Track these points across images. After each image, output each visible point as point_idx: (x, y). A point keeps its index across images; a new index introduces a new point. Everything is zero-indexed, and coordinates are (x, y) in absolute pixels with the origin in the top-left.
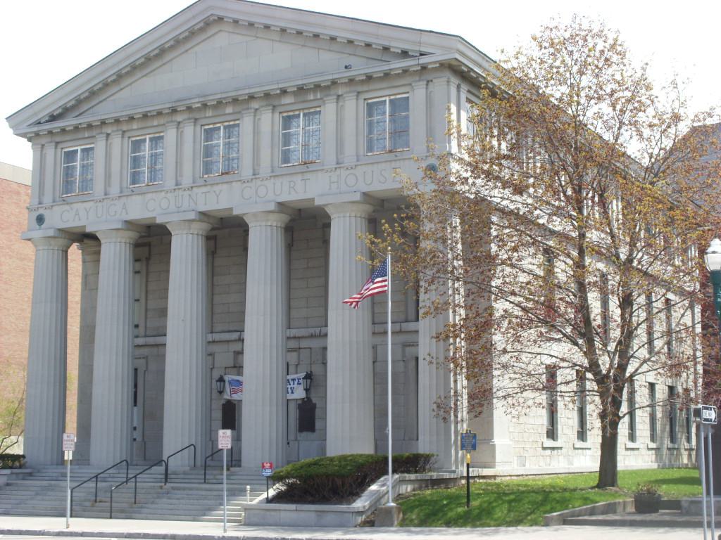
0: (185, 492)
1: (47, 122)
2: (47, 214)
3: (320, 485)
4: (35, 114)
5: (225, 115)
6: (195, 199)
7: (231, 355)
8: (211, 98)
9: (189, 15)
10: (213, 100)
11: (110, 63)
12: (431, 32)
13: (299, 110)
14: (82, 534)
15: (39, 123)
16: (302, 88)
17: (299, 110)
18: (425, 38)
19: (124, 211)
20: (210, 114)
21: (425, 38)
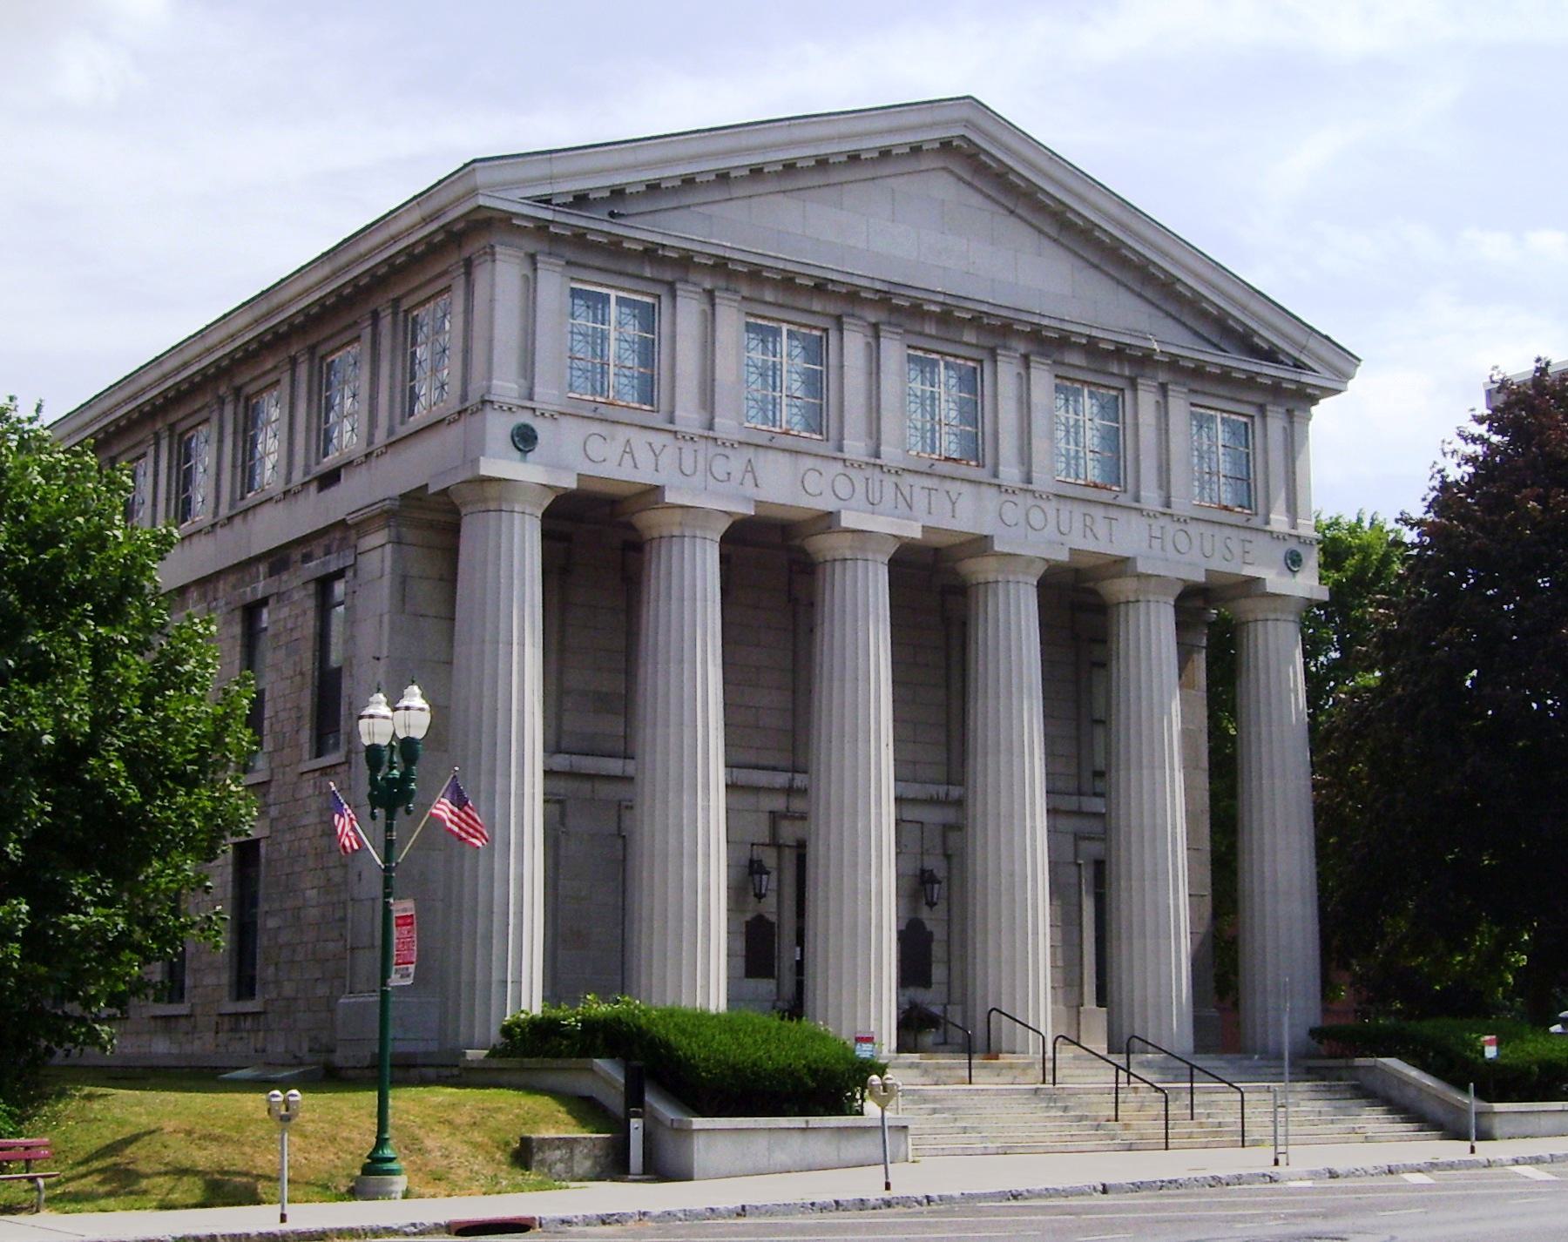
0: (1472, 1172)
1: (565, 205)
2: (542, 428)
3: (641, 1083)
4: (551, 179)
5: (1063, 364)
6: (900, 498)
7: (764, 821)
8: (1025, 317)
9: (927, 117)
10: (969, 310)
11: (746, 140)
12: (1327, 338)
13: (1085, 382)
14: (376, 1233)
15: (548, 202)
16: (792, 280)
17: (1085, 382)
18: (559, 167)
19: (749, 476)
20: (933, 332)
21: (1313, 344)
